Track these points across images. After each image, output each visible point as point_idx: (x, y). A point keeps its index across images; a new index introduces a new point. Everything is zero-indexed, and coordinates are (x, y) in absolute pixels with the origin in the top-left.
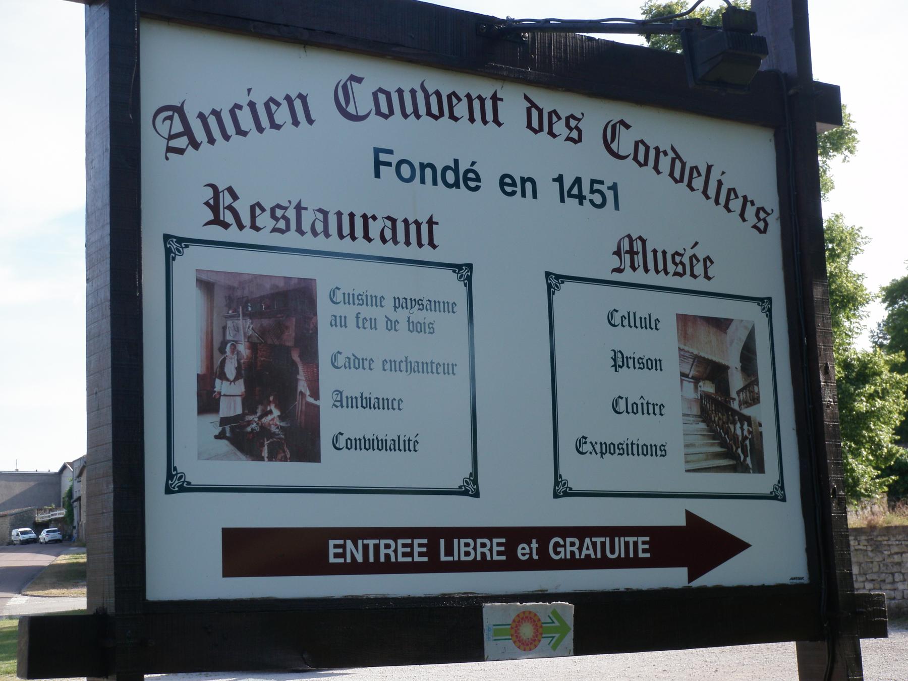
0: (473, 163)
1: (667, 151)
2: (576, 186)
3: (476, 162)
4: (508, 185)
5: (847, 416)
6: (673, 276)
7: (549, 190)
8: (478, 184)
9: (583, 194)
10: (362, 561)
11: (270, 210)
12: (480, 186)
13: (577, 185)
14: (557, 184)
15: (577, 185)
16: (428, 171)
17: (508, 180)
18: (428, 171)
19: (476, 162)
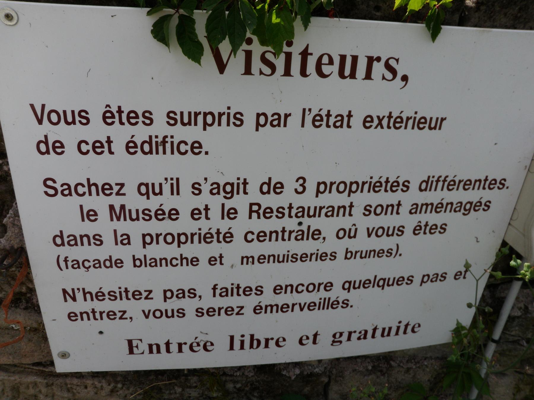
0: (133, 136)
1: (170, 137)
2: (302, 307)
3: (135, 135)
4: (92, 215)
5: (494, 360)
6: (111, 108)
7: (399, 325)
8: (96, 217)
9: (122, 110)
10: (130, 116)
11: (288, 232)
12: (199, 264)
13: (118, 216)
14: (484, 271)
15: (118, 216)
16: (70, 119)
17: (98, 144)
18: (70, 119)
19: (135, 135)
